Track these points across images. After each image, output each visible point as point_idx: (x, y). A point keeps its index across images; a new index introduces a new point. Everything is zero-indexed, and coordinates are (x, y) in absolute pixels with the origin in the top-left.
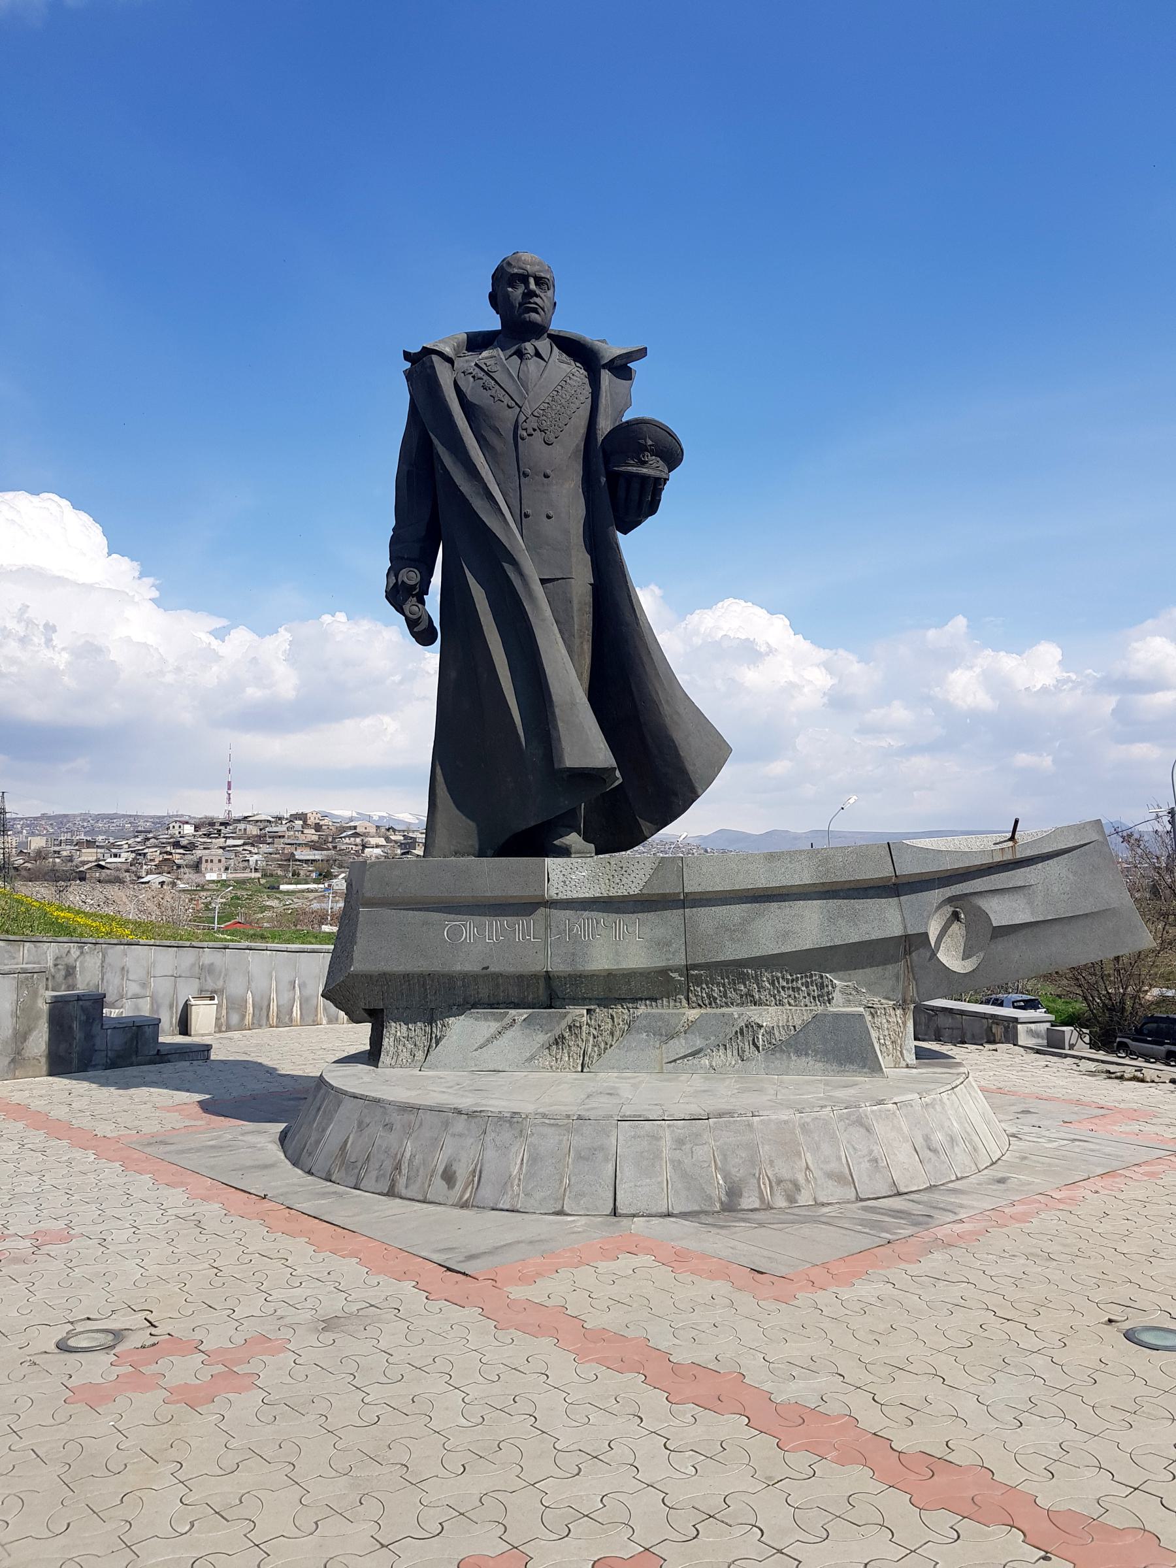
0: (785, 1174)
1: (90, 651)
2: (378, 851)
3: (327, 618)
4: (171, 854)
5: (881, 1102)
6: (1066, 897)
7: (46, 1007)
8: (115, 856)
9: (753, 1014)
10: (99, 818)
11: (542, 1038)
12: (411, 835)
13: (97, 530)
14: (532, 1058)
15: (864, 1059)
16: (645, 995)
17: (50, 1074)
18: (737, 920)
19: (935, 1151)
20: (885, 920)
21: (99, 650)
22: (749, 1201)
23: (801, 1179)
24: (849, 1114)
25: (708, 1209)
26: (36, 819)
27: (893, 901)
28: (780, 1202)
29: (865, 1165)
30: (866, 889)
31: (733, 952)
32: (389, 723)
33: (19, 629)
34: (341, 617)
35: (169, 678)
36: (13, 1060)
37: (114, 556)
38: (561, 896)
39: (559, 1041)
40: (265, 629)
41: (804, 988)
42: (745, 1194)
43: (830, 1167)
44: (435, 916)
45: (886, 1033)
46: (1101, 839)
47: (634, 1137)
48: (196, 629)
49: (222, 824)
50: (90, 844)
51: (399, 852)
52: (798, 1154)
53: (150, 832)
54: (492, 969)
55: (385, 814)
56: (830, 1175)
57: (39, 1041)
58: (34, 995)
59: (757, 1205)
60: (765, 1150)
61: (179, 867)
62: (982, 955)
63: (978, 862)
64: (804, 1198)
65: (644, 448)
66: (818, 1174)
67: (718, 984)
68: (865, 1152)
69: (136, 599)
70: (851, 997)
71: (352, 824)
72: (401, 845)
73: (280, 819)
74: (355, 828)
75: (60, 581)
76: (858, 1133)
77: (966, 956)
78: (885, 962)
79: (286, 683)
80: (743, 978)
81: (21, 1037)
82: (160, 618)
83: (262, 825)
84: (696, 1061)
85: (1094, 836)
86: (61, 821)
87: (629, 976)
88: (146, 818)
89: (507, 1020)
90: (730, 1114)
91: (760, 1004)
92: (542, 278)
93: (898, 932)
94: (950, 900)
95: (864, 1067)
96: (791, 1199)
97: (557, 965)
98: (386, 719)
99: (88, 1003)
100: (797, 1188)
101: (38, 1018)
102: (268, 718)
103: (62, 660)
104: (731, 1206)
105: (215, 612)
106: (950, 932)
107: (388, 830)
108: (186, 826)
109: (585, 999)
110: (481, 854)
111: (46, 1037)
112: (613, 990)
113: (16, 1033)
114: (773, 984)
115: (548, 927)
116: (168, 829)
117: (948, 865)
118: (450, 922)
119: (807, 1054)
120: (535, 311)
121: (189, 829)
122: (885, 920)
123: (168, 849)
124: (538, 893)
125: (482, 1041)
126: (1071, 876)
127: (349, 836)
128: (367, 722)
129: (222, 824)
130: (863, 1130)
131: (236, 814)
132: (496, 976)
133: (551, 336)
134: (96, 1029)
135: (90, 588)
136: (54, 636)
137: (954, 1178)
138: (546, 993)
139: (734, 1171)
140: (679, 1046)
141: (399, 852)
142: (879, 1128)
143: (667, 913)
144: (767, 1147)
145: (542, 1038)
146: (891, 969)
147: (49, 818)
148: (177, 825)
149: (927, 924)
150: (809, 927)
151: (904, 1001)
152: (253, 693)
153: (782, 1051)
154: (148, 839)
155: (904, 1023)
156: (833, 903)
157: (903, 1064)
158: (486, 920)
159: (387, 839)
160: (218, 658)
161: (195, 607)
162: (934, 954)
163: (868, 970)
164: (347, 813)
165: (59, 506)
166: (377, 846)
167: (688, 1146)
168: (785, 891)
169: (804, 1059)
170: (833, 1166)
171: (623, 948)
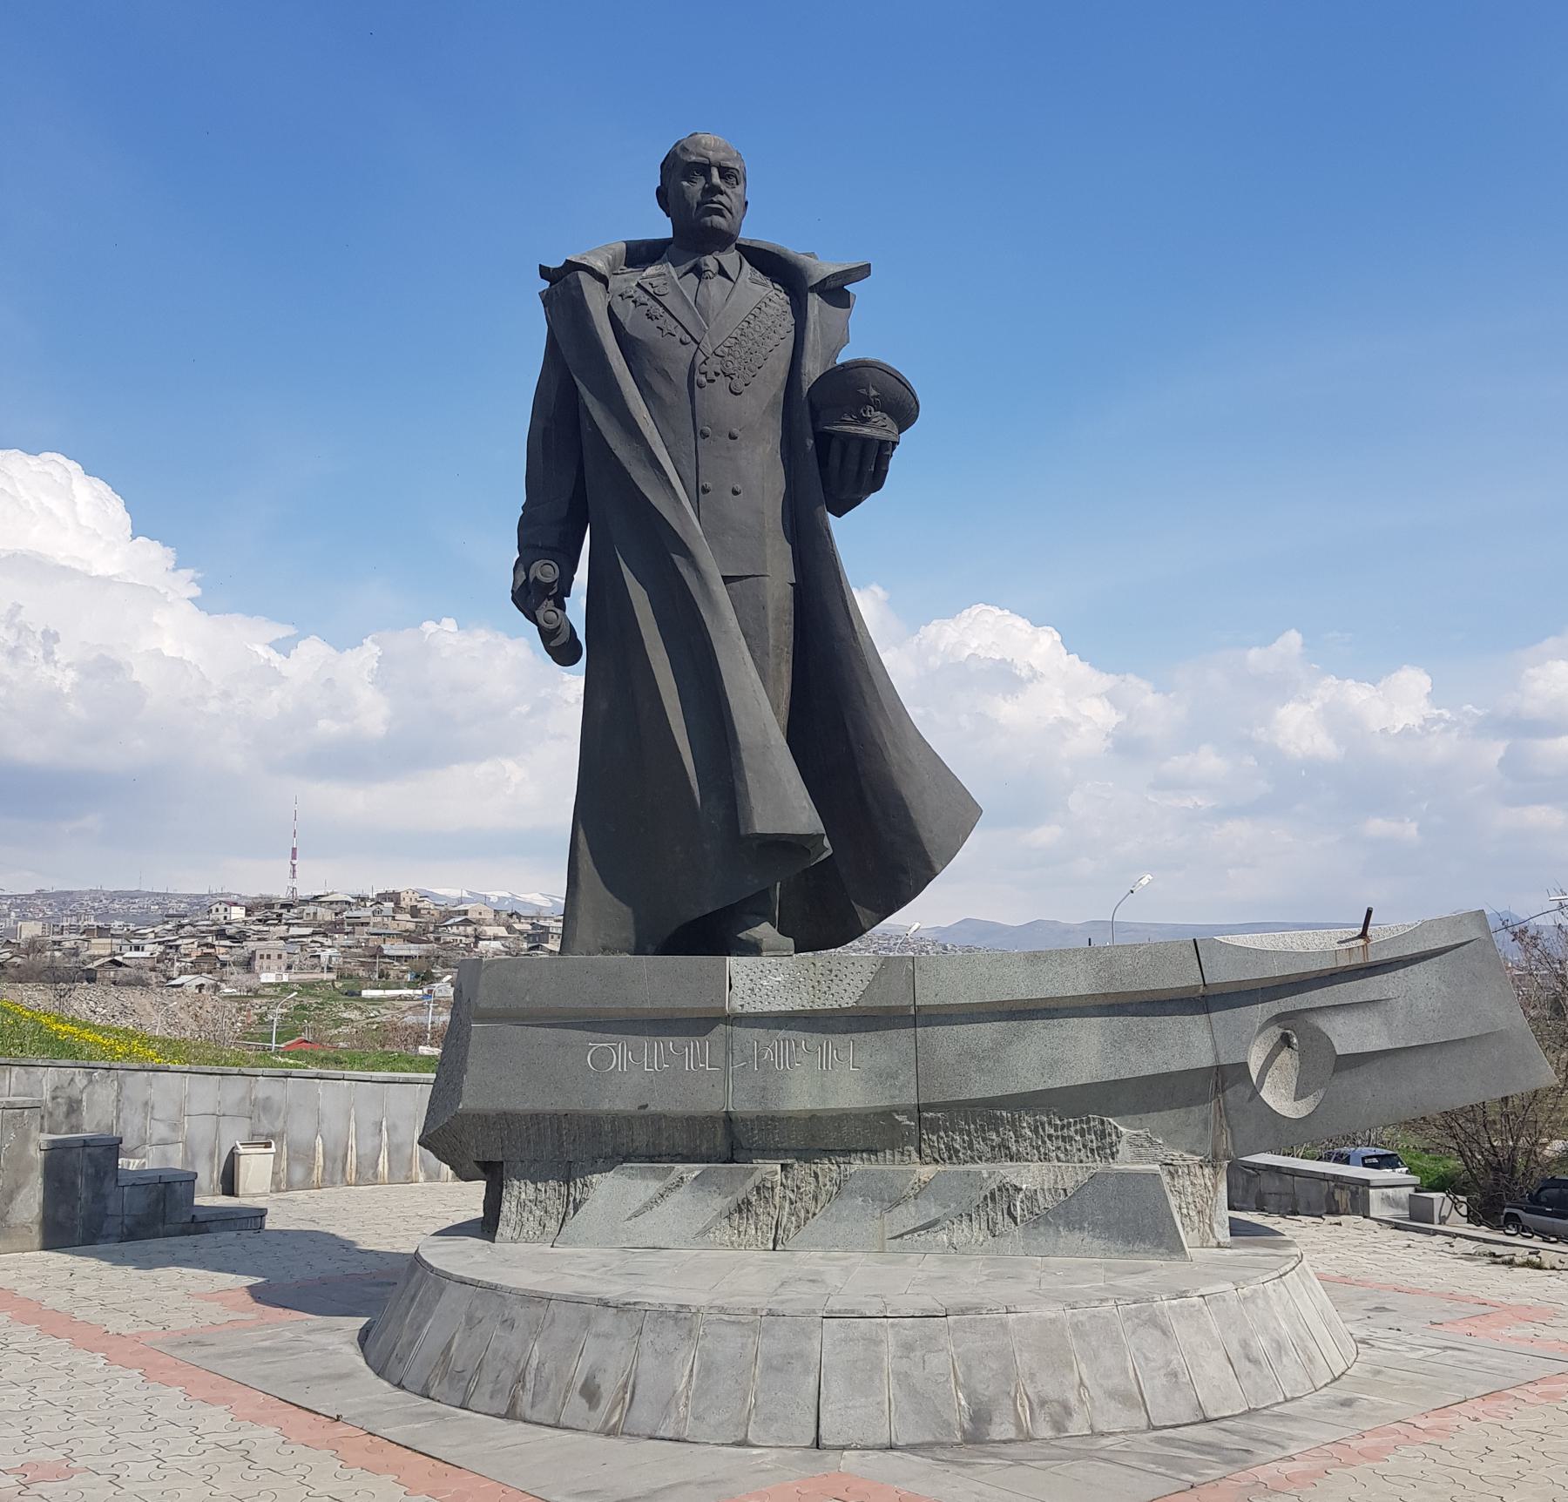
0: (1051, 1391)
1: (105, 667)
2: (497, 945)
3: (430, 627)
4: (213, 946)
5: (1182, 1295)
6: (1436, 1015)
7: (40, 1156)
8: (137, 949)
9: (1009, 1172)
11: (720, 1203)
12: (541, 923)
14: (706, 1231)
16: (861, 1145)
18: (987, 1044)
19: (1255, 1362)
20: (1189, 1045)
22: (1002, 1429)
24: (1139, 1311)
26: (29, 897)
28: (1045, 1431)
31: (981, 1087)
34: (449, 624)
35: (213, 706)
37: (140, 539)
38: (747, 1009)
39: (743, 1207)
40: (343, 641)
41: (1078, 1138)
42: (996, 1419)
47: (845, 1340)
48: (250, 640)
49: (283, 906)
50: (103, 932)
51: (525, 945)
56: (1112, 1394)
57: (30, 1203)
60: (1024, 1360)
61: (224, 964)
62: (1321, 1093)
64: (1077, 1425)
65: (867, 401)
66: (1096, 1392)
70: (1142, 1150)
71: (462, 907)
72: (529, 937)
73: (363, 899)
74: (466, 912)
79: (373, 714)
83: (338, 908)
85: (1475, 933)
86: (63, 899)
87: (840, 1118)
88: (179, 898)
89: (673, 1178)
90: (977, 1310)
93: (1207, 1061)
94: (1278, 1019)
95: (1158, 1246)
96: (1059, 1427)
98: (509, 765)
99: (99, 1151)
100: (1067, 1410)
102: (349, 761)
103: (66, 679)
104: (976, 1436)
107: (511, 916)
108: (235, 909)
109: (779, 1150)
110: (639, 950)
111: (39, 1196)
112: (875, 1133)
115: (729, 1051)
116: (210, 912)
117: (1276, 970)
118: (597, 1043)
119: (1082, 1229)
121: (238, 913)
122: (1189, 1045)
123: (210, 940)
125: (638, 1206)
128: (484, 767)
129: (283, 906)
130: (1158, 1333)
132: (658, 1118)
134: (109, 1185)
135: (107, 581)
137: (1281, 1399)
138: (725, 1142)
139: (980, 1387)
140: (907, 1216)
141: (525, 945)
142: (1179, 1329)
143: (892, 1033)
145: (720, 1203)
147: (47, 896)
149: (1246, 1051)
150: (1086, 1053)
151: (1215, 1156)
153: (1048, 1223)
154: (182, 926)
155: (1215, 1187)
156: (1118, 1021)
157: (1213, 1242)
159: (510, 929)
162: (1255, 1093)
163: (1166, 1114)
166: (496, 938)
168: (1053, 1005)
169: (1077, 1234)
171: (830, 1080)
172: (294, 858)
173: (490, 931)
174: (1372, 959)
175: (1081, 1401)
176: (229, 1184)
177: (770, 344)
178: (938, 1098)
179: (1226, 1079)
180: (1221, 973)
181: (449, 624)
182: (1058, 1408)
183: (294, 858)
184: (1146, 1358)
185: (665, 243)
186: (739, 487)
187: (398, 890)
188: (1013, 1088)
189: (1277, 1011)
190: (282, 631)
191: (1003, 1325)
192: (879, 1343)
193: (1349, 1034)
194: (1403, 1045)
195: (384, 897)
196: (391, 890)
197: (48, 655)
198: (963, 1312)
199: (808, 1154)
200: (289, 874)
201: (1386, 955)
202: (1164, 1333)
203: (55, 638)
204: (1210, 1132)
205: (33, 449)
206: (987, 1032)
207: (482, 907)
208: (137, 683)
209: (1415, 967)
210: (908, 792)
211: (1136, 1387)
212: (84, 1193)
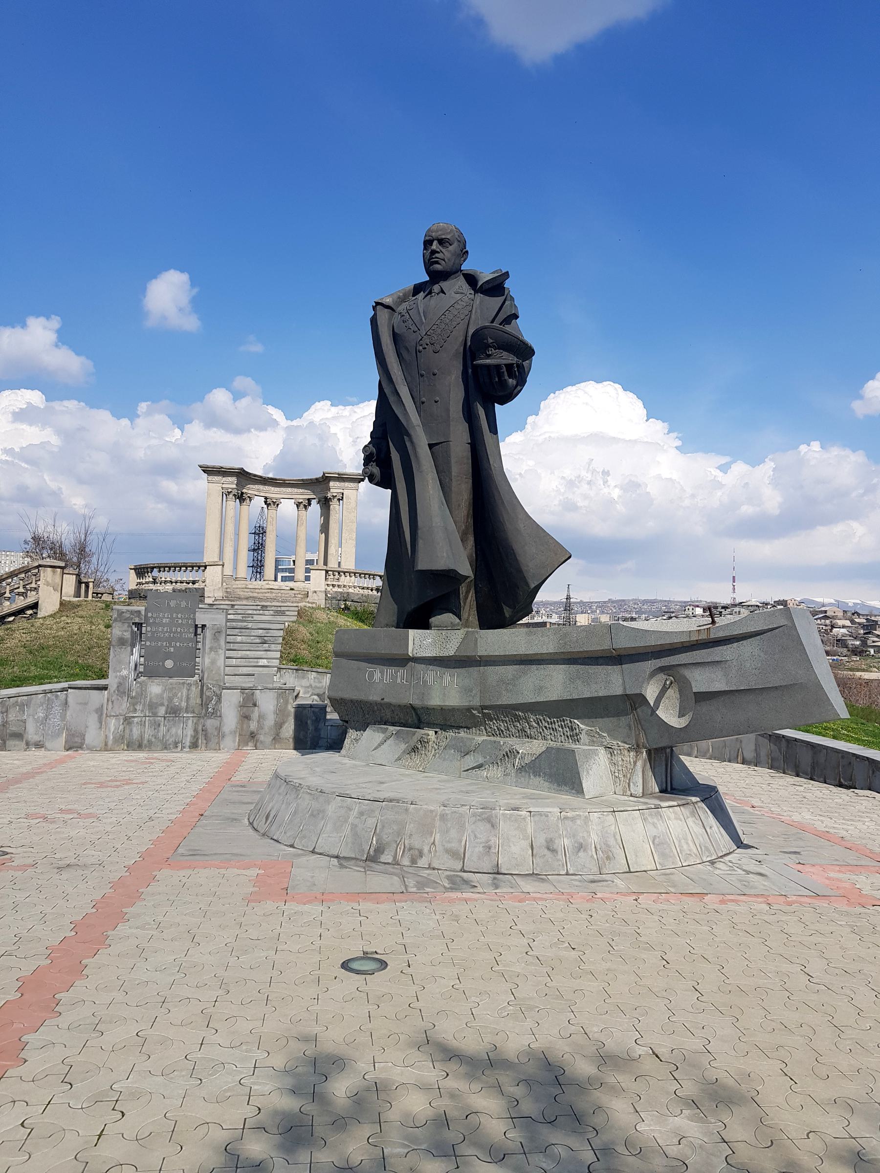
1: (631, 486)
3: (803, 448)
5: (516, 809)
6: (757, 672)
7: (293, 710)
10: (645, 602)
11: (403, 746)
12: (873, 618)
13: (640, 404)
14: (399, 759)
17: (295, 749)
18: (510, 676)
19: (554, 851)
20: (611, 682)
21: (639, 485)
22: (387, 857)
24: (482, 813)
26: (605, 602)
27: (617, 668)
28: (406, 862)
29: (480, 849)
30: (597, 658)
32: (858, 528)
33: (589, 476)
34: (816, 446)
35: (687, 503)
38: (418, 655)
39: (415, 750)
40: (755, 461)
43: (448, 846)
46: (790, 624)
47: (340, 807)
48: (706, 466)
49: (723, 608)
51: (862, 632)
52: (431, 833)
53: (673, 612)
56: (447, 851)
57: (289, 729)
59: (390, 861)
60: (410, 827)
62: (691, 714)
63: (685, 639)
64: (423, 862)
65: (488, 346)
66: (439, 848)
68: (483, 840)
69: (665, 447)
71: (823, 609)
72: (864, 626)
73: (766, 604)
74: (826, 612)
75: (615, 440)
76: (483, 827)
79: (772, 501)
80: (518, 719)
81: (279, 725)
82: (681, 460)
83: (752, 609)
85: (783, 622)
86: (621, 603)
87: (453, 710)
90: (398, 801)
91: (531, 738)
92: (442, 239)
93: (619, 691)
94: (662, 669)
95: (572, 789)
96: (413, 861)
97: (413, 700)
98: (855, 525)
100: (421, 854)
101: (288, 716)
102: (760, 528)
103: (616, 493)
104: (373, 858)
107: (853, 614)
111: (293, 727)
112: (447, 720)
113: (276, 724)
114: (538, 724)
117: (652, 642)
118: (369, 668)
119: (539, 775)
120: (437, 263)
122: (611, 682)
124: (405, 652)
125: (376, 744)
126: (762, 654)
127: (820, 619)
128: (839, 528)
129: (723, 608)
130: (488, 826)
132: (389, 705)
134: (321, 725)
135: (635, 442)
137: (564, 872)
138: (413, 718)
139: (385, 837)
140: (471, 761)
141: (862, 632)
143: (471, 669)
145: (403, 746)
146: (624, 721)
147: (613, 602)
149: (641, 687)
150: (555, 683)
151: (638, 746)
152: (747, 510)
153: (526, 771)
155: (635, 763)
156: (573, 668)
157: (629, 793)
159: (852, 622)
160: (720, 485)
162: (653, 712)
164: (827, 600)
166: (844, 627)
168: (539, 657)
169: (538, 779)
170: (454, 845)
171: (447, 691)
173: (840, 623)
174: (712, 636)
175: (430, 851)
176: (436, 732)
177: (455, 323)
179: (633, 703)
180: (623, 643)
181: (816, 446)
182: (417, 852)
184: (475, 836)
186: (437, 399)
187: (786, 599)
188: (521, 700)
189: (660, 665)
191: (407, 810)
192: (350, 810)
193: (702, 680)
194: (735, 688)
195: (779, 603)
196: (782, 599)
197: (605, 482)
198: (391, 801)
199: (445, 727)
200: (731, 590)
201: (721, 634)
202: (493, 826)
206: (509, 671)
207: (836, 609)
208: (648, 493)
209: (744, 642)
210: (517, 547)
211: (462, 850)
212: (311, 727)
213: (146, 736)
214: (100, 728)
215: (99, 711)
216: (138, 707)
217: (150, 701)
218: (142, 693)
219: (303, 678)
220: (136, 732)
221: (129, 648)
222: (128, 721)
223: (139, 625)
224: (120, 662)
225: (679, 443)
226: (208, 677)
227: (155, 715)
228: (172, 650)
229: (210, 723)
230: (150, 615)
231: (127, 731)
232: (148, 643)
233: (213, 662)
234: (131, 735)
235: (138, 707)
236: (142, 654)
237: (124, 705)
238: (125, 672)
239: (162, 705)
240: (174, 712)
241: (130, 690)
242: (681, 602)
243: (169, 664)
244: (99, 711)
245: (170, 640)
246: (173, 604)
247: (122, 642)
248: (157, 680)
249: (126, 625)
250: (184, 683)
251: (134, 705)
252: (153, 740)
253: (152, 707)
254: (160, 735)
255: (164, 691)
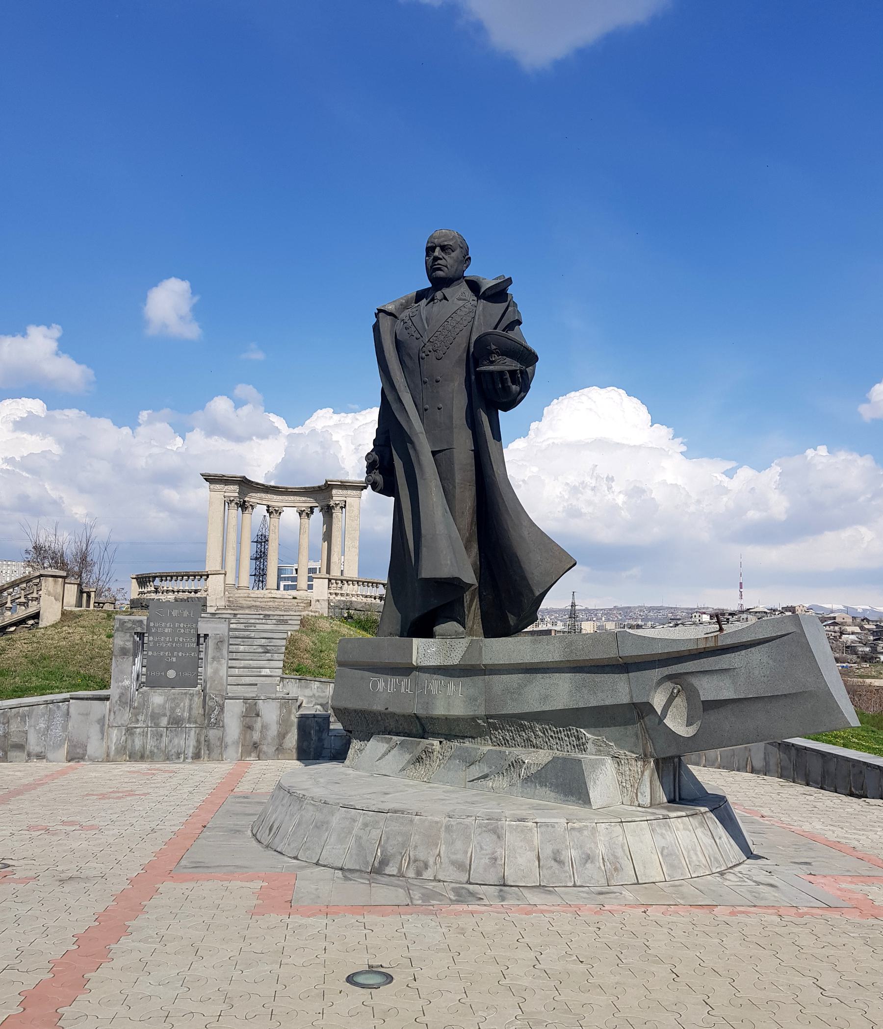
0: (422, 856)
1: (636, 492)
2: (853, 637)
3: (810, 452)
7: (296, 720)
9: (518, 752)
10: (651, 609)
11: (408, 757)
13: (644, 409)
14: (403, 769)
15: (580, 793)
16: (469, 734)
18: (515, 685)
19: (560, 862)
20: (617, 690)
21: (643, 491)
22: (391, 869)
23: (431, 861)
24: (488, 824)
25: (363, 869)
26: (610, 610)
27: (624, 676)
28: (411, 874)
31: (511, 708)
33: (593, 483)
34: (823, 450)
35: (692, 509)
36: (277, 749)
39: (419, 760)
40: (760, 467)
41: (567, 739)
42: (391, 865)
44: (367, 673)
45: (628, 778)
47: (344, 818)
48: (711, 471)
49: (730, 614)
51: (872, 638)
53: (679, 619)
54: (389, 710)
55: (868, 608)
56: (453, 863)
58: (290, 712)
60: (415, 839)
62: (699, 723)
64: (428, 874)
66: (445, 860)
67: (508, 730)
70: (602, 749)
71: (832, 615)
72: (873, 633)
73: (774, 611)
74: (834, 618)
75: (619, 446)
77: (689, 724)
78: (626, 723)
79: (779, 506)
80: (523, 728)
81: (282, 736)
82: (687, 465)
84: (484, 783)
85: (791, 629)
87: (458, 719)
88: (682, 610)
89: (392, 744)
92: (445, 246)
93: (626, 700)
94: (670, 678)
95: (579, 799)
96: (419, 873)
98: (863, 529)
99: (320, 720)
100: (426, 866)
101: (292, 725)
103: (620, 499)
104: (378, 870)
105: (726, 457)
106: (674, 703)
107: (863, 620)
108: (704, 616)
109: (439, 734)
110: (401, 636)
111: (296, 737)
112: (451, 730)
113: (279, 734)
115: (416, 684)
117: (659, 649)
118: (373, 677)
119: (546, 785)
122: (617, 690)
125: (380, 755)
126: (771, 662)
127: (829, 625)
128: (846, 534)
129: (730, 614)
130: (495, 837)
131: (745, 607)
133: (467, 281)
134: (325, 735)
135: (638, 448)
136: (613, 484)
137: (571, 884)
138: (417, 728)
139: (390, 848)
140: (476, 771)
141: (872, 638)
142: (509, 837)
143: (476, 678)
144: (417, 837)
145: (408, 757)
146: (631, 730)
147: (619, 609)
148: (697, 615)
149: (648, 695)
150: (561, 693)
151: (645, 755)
152: (753, 515)
153: (532, 781)
155: (643, 772)
156: (579, 676)
157: (636, 803)
158: (389, 678)
159: (862, 628)
161: (711, 456)
162: (661, 721)
163: (613, 729)
164: (835, 607)
165: (620, 394)
166: (853, 633)
167: (369, 828)
170: (459, 857)
171: (451, 700)
172: (741, 588)
173: (849, 629)
174: (720, 644)
175: (435, 863)
176: (441, 742)
177: (458, 330)
178: (493, 713)
179: (640, 711)
180: (629, 651)
181: (823, 450)
182: (422, 864)
183: (741, 588)
185: (428, 289)
186: (441, 405)
187: (794, 605)
188: (527, 709)
189: (667, 673)
190: (729, 465)
191: (412, 821)
192: (354, 821)
193: (711, 689)
195: (787, 609)
198: (396, 812)
199: (449, 737)
200: (739, 597)
201: (729, 641)
202: (499, 837)
203: (612, 479)
204: (640, 741)
205: (602, 386)
206: (516, 678)
207: (844, 615)
209: (753, 649)
210: (521, 554)
211: (468, 862)
212: (314, 738)
213: (148, 747)
214: (102, 739)
215: (101, 721)
216: (140, 718)
217: (153, 710)
218: (145, 703)
219: (306, 687)
220: (138, 743)
221: (131, 658)
222: (130, 731)
223: (141, 635)
224: (122, 672)
225: (684, 448)
226: (211, 687)
227: (157, 725)
228: (174, 660)
229: (213, 733)
230: (152, 624)
231: (129, 742)
232: (150, 653)
233: (216, 672)
234: (133, 746)
235: (140, 718)
236: (145, 664)
237: (126, 716)
238: (127, 683)
239: (165, 715)
240: (176, 722)
241: (132, 700)
242: (687, 609)
243: (171, 674)
244: (101, 721)
245: (172, 650)
246: (175, 613)
247: (124, 652)
248: (159, 691)
249: (128, 635)
250: (185, 694)
251: (136, 715)
252: (156, 751)
253: (155, 717)
254: (163, 745)
255: (165, 702)
